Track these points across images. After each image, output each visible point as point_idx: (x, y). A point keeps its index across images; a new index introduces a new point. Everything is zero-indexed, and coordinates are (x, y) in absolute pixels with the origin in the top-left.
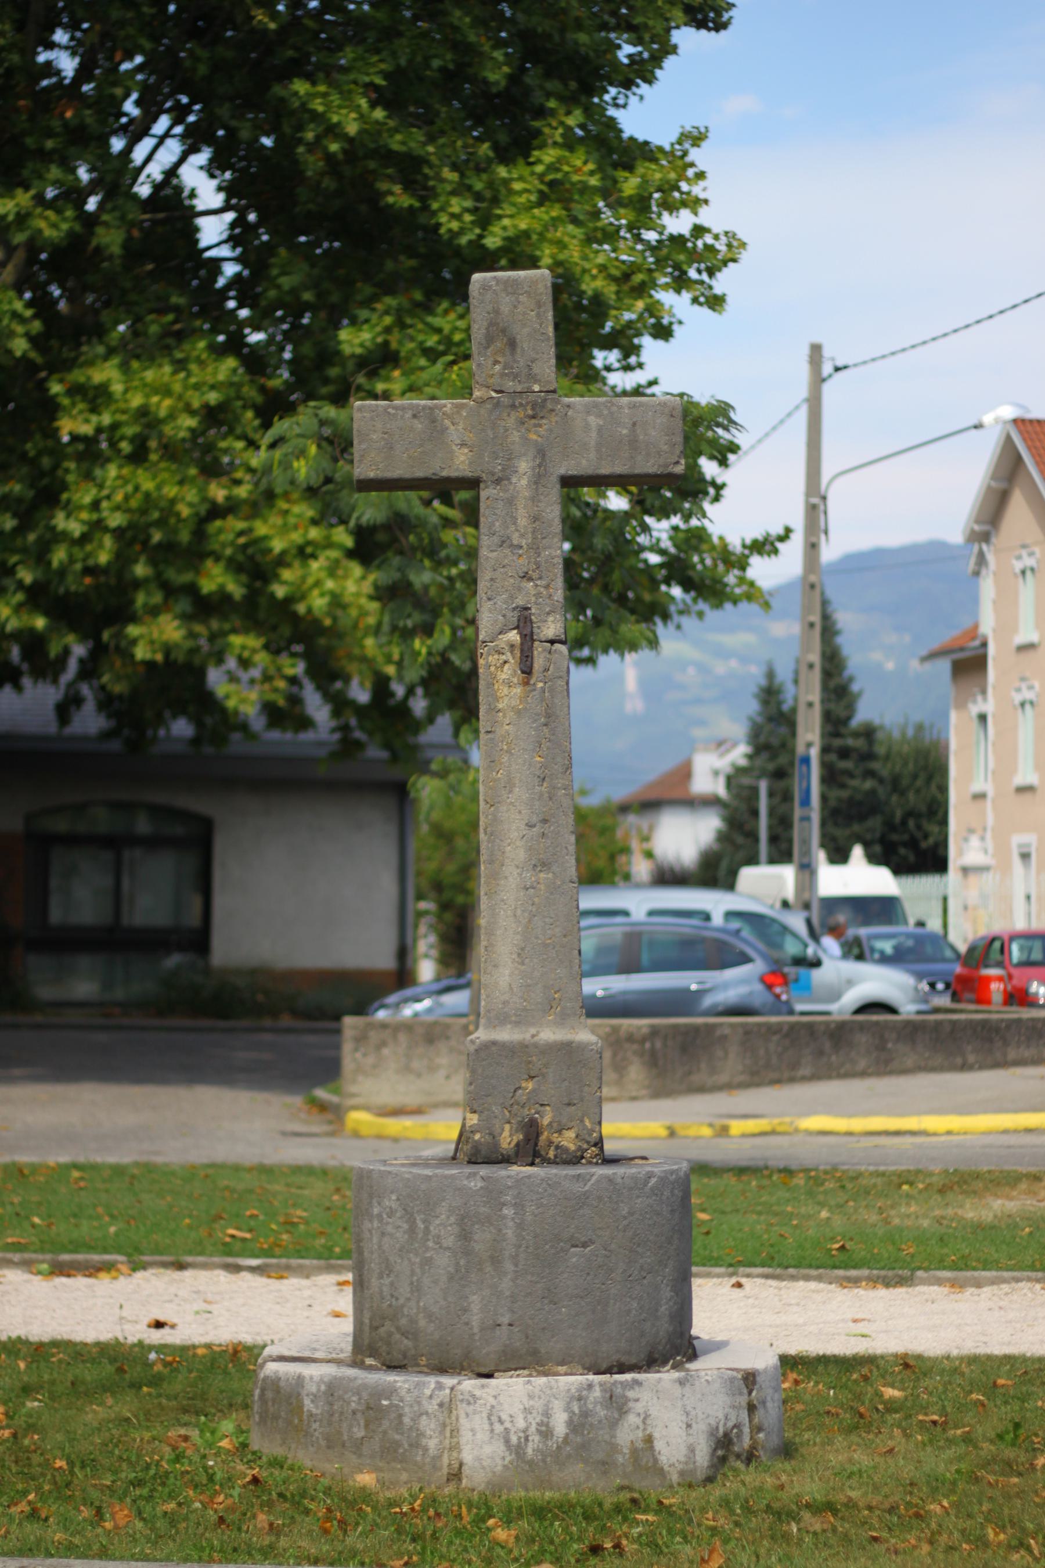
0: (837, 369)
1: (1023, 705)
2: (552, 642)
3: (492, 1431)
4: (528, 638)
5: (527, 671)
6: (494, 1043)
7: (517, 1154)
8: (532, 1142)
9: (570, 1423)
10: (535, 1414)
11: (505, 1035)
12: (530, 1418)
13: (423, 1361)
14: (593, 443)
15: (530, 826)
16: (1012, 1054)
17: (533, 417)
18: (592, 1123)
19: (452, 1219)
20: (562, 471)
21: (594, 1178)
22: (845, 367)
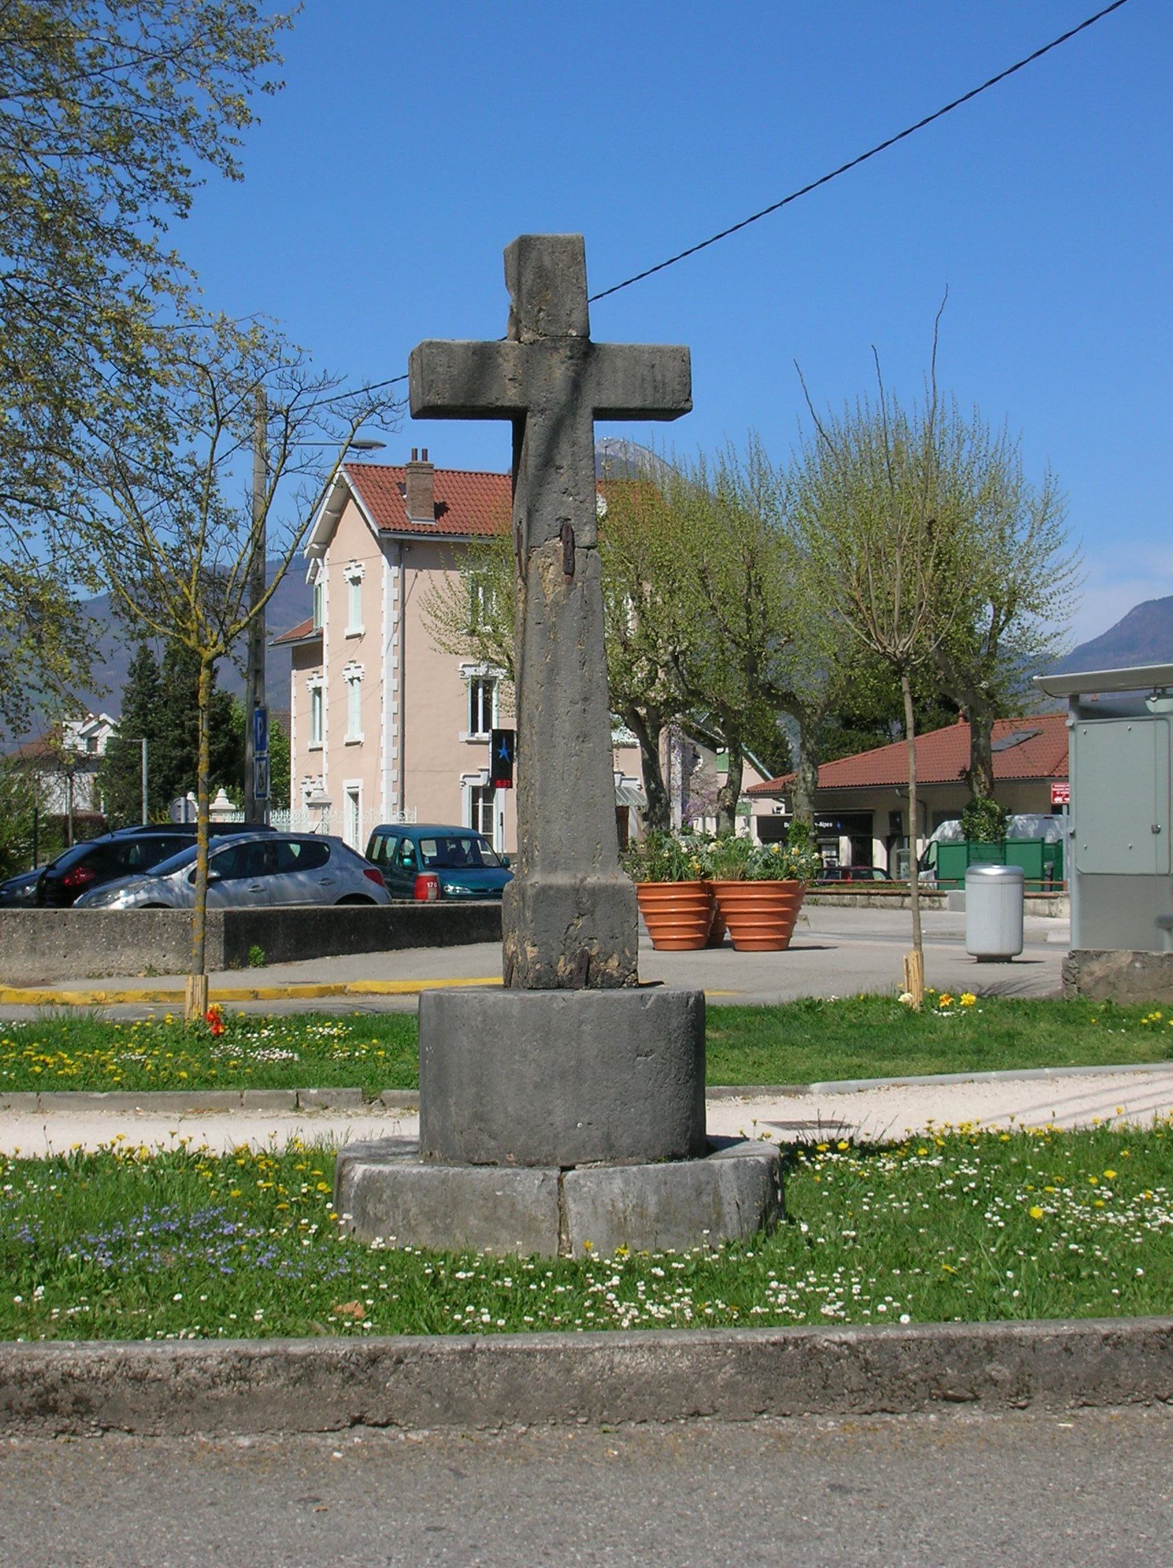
1: (351, 680)
2: (589, 548)
3: (596, 1212)
4: (570, 545)
5: (570, 571)
6: (550, 887)
7: (571, 980)
8: (584, 971)
9: (659, 1203)
11: (562, 879)
12: (627, 1201)
13: (512, 1158)
15: (574, 703)
19: (538, 1036)
21: (653, 998)
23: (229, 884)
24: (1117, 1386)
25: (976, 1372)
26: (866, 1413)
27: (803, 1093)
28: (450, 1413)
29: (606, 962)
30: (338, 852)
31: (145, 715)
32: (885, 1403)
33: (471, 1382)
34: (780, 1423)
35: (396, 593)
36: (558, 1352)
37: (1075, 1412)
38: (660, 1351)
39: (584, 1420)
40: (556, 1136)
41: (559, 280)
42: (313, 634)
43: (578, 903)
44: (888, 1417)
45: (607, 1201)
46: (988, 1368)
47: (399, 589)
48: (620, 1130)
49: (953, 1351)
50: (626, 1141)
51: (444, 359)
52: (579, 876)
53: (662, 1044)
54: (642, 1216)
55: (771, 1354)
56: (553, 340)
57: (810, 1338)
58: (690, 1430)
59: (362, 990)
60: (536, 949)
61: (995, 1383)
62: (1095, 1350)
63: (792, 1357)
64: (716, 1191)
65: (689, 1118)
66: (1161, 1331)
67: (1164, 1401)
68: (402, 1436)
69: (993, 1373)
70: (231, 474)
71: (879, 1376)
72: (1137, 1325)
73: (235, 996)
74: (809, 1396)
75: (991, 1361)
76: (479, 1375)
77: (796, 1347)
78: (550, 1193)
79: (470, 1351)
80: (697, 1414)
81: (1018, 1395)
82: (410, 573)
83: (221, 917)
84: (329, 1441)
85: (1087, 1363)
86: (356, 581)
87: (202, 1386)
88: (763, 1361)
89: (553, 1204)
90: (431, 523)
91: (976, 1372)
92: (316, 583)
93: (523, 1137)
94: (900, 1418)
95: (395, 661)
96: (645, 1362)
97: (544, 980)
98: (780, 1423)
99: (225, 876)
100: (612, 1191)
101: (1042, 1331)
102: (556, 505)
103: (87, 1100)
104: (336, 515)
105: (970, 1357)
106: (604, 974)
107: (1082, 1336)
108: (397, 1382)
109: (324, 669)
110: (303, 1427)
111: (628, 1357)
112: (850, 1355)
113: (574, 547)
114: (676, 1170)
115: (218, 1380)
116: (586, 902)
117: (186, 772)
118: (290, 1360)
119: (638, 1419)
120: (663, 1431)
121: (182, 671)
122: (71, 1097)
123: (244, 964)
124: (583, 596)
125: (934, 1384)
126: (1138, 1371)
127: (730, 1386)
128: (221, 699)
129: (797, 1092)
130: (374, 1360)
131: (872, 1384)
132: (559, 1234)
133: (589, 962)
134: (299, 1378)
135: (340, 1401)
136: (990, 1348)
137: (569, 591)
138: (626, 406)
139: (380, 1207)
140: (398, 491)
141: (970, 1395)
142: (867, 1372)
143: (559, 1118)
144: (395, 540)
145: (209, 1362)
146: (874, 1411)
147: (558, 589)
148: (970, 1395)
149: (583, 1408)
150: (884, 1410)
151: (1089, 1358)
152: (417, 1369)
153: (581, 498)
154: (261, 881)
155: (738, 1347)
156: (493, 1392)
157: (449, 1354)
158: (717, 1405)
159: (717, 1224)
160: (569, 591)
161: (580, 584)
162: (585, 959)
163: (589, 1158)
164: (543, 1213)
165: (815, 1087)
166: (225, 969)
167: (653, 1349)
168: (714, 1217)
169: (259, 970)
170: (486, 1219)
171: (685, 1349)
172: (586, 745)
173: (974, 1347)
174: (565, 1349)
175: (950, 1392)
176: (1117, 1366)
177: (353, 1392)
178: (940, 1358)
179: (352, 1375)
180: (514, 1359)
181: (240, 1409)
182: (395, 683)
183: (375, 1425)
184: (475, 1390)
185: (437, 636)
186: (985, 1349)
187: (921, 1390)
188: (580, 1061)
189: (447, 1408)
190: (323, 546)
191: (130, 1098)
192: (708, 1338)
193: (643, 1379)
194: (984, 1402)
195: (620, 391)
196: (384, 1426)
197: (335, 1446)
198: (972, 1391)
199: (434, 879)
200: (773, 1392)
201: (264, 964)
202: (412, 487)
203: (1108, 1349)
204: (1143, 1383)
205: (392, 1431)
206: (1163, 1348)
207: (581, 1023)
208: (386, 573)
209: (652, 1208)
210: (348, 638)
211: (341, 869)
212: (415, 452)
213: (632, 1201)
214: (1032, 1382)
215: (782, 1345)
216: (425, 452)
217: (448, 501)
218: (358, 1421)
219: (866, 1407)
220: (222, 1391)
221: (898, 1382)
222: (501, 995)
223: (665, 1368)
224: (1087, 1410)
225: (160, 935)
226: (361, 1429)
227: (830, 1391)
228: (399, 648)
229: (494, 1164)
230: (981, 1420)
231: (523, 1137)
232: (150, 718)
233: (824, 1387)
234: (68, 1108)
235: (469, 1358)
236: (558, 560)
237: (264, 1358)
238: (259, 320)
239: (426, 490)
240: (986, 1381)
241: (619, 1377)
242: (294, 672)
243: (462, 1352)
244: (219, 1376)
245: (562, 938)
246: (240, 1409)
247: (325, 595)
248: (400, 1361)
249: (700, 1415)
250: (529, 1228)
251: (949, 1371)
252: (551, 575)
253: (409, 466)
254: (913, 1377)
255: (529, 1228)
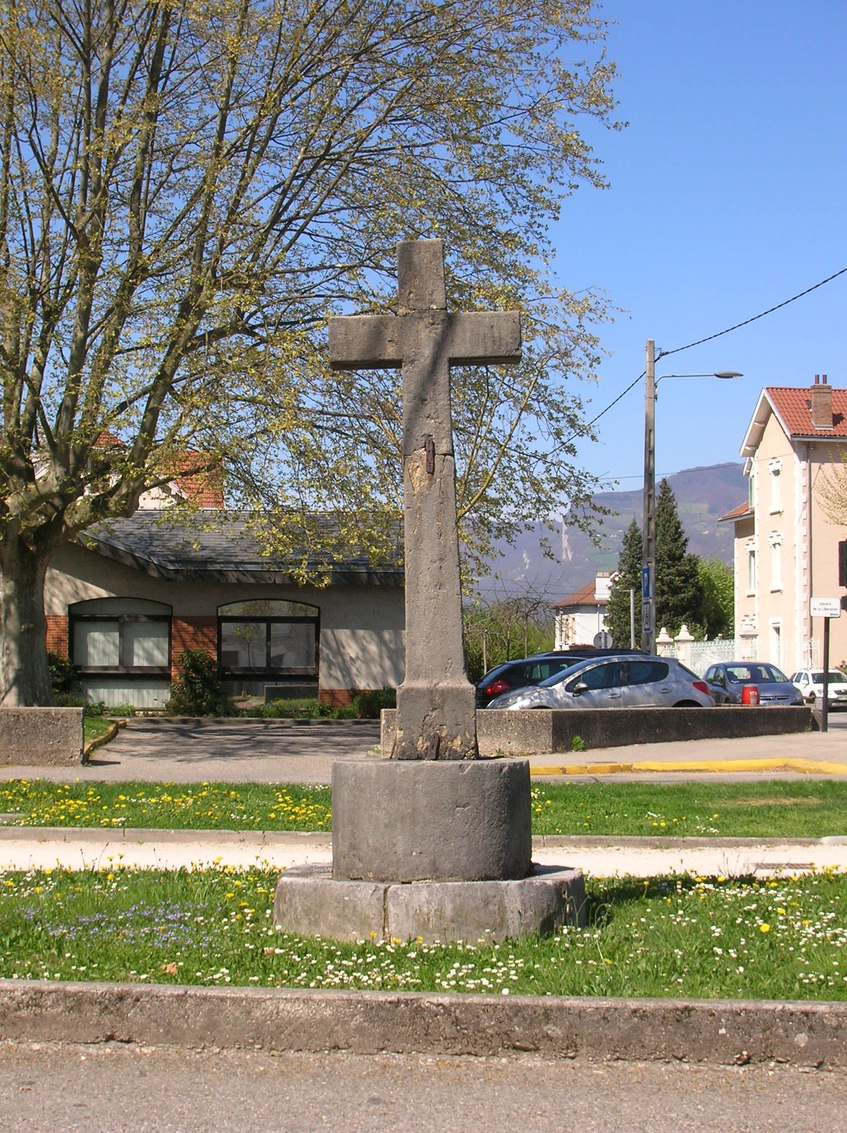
0: (662, 355)
1: (774, 545)
2: (445, 455)
3: (408, 914)
5: (432, 472)
6: (412, 689)
7: (426, 754)
8: (435, 747)
9: (454, 909)
10: (433, 904)
13: (371, 875)
14: (468, 339)
15: (433, 562)
16: (761, 729)
17: (433, 324)
18: (471, 736)
19: (387, 792)
20: (450, 355)
22: (667, 353)
23: (595, 692)
24: (643, 1047)
25: (537, 1031)
26: (456, 1054)
27: (815, 844)
28: (170, 1037)
29: (452, 741)
30: (675, 671)
31: (635, 573)
32: (470, 1048)
33: (183, 1016)
34: (394, 1057)
35: (804, 481)
36: (242, 1000)
37: (610, 1063)
38: (311, 1003)
39: (259, 1046)
40: (398, 861)
41: (423, 272)
42: (749, 512)
43: (432, 701)
44: (472, 1058)
45: (416, 906)
46: (545, 1028)
47: (807, 477)
48: (443, 858)
49: (519, 1014)
50: (447, 866)
51: (343, 330)
52: (435, 682)
53: (477, 800)
54: (441, 917)
55: (389, 1010)
56: (420, 313)
57: (418, 1000)
58: (329, 1058)
59: (643, 768)
60: (402, 732)
61: (551, 1039)
62: (626, 1020)
63: (403, 1013)
64: (501, 903)
65: (501, 851)
66: (677, 1009)
67: (680, 1059)
68: (138, 1050)
69: (549, 1032)
70: (591, 401)
71: (466, 1029)
72: (660, 1003)
73: (549, 771)
74: (416, 1040)
75: (548, 1023)
76: (189, 1012)
77: (407, 1005)
78: (378, 899)
79: (183, 996)
80: (337, 1047)
81: (568, 1048)
82: (815, 466)
83: (550, 716)
84: (91, 1050)
85: (620, 1029)
86: (777, 473)
87: (11, 1009)
88: (382, 1014)
89: (380, 907)
90: (829, 429)
91: (537, 1031)
92: (751, 475)
93: (377, 862)
94: (480, 1059)
95: (805, 530)
96: (301, 1010)
97: (407, 753)
98: (394, 1057)
99: (591, 687)
100: (420, 899)
101: (586, 1004)
102: (427, 426)
103: (297, 837)
104: (763, 425)
105: (532, 1020)
106: (450, 750)
107: (616, 1009)
108: (136, 1013)
109: (755, 537)
110: (75, 1039)
111: (289, 1006)
112: (445, 1013)
113: (434, 454)
114: (469, 886)
115: (21, 1005)
116: (438, 699)
117: (665, 613)
118: (67, 995)
119: (296, 1048)
120: (312, 1057)
121: (661, 540)
122: (285, 834)
123: (568, 748)
124: (440, 488)
125: (505, 1037)
126: (658, 1037)
127: (359, 1030)
128: (690, 560)
129: (811, 843)
130: (121, 998)
131: (459, 1035)
132: (384, 928)
133: (439, 742)
134: (72, 1008)
135: (98, 1024)
136: (547, 1014)
137: (430, 485)
138: (472, 355)
139: (285, 905)
140: (806, 406)
141: (532, 1046)
142: (457, 1025)
143: (400, 849)
144: (804, 443)
145: (16, 993)
146: (463, 1054)
147: (423, 484)
148: (532, 1046)
149: (258, 1038)
150: (469, 1053)
151: (621, 1025)
152: (148, 1006)
153: (439, 420)
154: (617, 690)
155: (366, 1004)
156: (198, 1024)
157: (169, 997)
158: (350, 1042)
159: (501, 924)
160: (430, 485)
161: (438, 480)
162: (437, 739)
163: (421, 877)
164: (373, 912)
165: (825, 840)
166: (553, 752)
167: (306, 1001)
168: (498, 920)
169: (579, 753)
170: (338, 916)
171: (329, 1003)
172: (441, 591)
173: (535, 1012)
174: (246, 998)
175: (517, 1043)
176: (642, 1032)
177: (107, 1019)
178: (510, 1019)
179: (106, 1007)
180: (212, 1003)
181: (35, 1025)
182: (805, 547)
183: (122, 1041)
184: (186, 1022)
185: (828, 511)
186: (543, 1014)
187: (496, 1041)
188: (414, 810)
189: (168, 1033)
190: (754, 448)
191: (326, 836)
192: (345, 996)
193: (299, 1021)
194: (543, 1052)
195: (468, 345)
196: (128, 1042)
197: (85, 1053)
198: (533, 1043)
199: (755, 689)
200: (390, 1036)
201: (584, 749)
202: (816, 403)
203: (636, 1019)
204: (663, 1046)
205: (132, 1046)
206: (678, 1021)
207: (416, 783)
208: (795, 466)
209: (449, 911)
210: (772, 514)
211: (677, 682)
212: (817, 377)
213: (434, 907)
214: (578, 1041)
215: (398, 1003)
216: (825, 377)
217: (843, 413)
218: (110, 1038)
219: (456, 1050)
220: (24, 1013)
221: (480, 1034)
222: (388, 763)
223: (315, 1014)
224: (620, 1063)
225: (507, 728)
226: (112, 1043)
227: (430, 1038)
228: (807, 522)
229: (361, 879)
230: (539, 1064)
231: (377, 862)
232: (639, 575)
233: (426, 1035)
234: (284, 842)
235: (182, 1000)
236: (422, 463)
237: (50, 992)
238: (592, 291)
239: (826, 405)
240: (544, 1037)
241: (283, 1019)
242: (736, 540)
243: (178, 996)
244: (22, 1003)
245: (420, 725)
246: (35, 1025)
247: (756, 484)
248: (138, 1000)
249: (339, 1048)
250: (364, 923)
251: (517, 1029)
252: (417, 474)
253: (813, 388)
254: (490, 1031)
255: (364, 923)
